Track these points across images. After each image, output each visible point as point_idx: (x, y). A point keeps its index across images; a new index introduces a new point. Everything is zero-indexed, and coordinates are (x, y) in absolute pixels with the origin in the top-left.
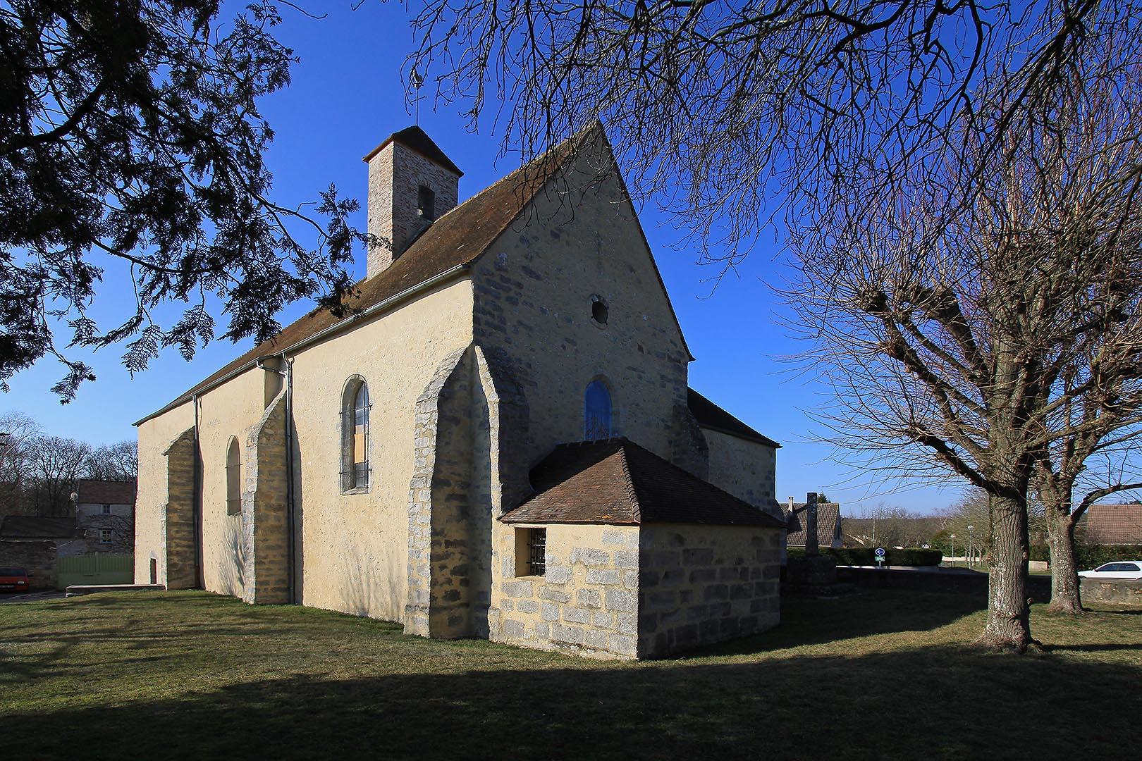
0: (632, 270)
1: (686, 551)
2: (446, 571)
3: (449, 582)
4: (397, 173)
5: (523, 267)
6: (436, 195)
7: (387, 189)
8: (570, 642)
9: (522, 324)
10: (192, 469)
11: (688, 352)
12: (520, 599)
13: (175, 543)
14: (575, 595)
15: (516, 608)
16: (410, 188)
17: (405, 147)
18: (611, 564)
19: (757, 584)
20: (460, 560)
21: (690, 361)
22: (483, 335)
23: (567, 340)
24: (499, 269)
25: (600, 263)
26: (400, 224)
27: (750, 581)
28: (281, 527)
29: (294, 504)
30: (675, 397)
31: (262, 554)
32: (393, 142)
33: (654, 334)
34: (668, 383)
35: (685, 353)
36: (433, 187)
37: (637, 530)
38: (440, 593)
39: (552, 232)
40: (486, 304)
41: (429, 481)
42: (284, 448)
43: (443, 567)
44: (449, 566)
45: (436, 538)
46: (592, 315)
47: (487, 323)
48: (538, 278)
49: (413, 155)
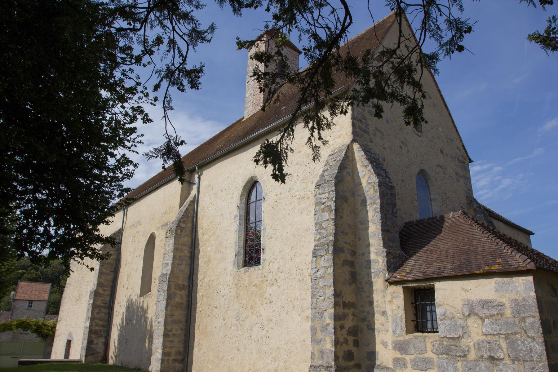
9: (377, 129)
10: (114, 262)
11: (468, 156)
12: (412, 357)
13: (95, 322)
14: (472, 348)
15: (409, 365)
18: (508, 313)
22: (358, 136)
28: (182, 303)
29: (193, 284)
31: (169, 328)
34: (460, 178)
35: (467, 157)
37: (530, 278)
38: (341, 354)
40: (358, 114)
41: (331, 248)
42: (190, 238)
43: (342, 327)
44: (345, 326)
47: (360, 128)
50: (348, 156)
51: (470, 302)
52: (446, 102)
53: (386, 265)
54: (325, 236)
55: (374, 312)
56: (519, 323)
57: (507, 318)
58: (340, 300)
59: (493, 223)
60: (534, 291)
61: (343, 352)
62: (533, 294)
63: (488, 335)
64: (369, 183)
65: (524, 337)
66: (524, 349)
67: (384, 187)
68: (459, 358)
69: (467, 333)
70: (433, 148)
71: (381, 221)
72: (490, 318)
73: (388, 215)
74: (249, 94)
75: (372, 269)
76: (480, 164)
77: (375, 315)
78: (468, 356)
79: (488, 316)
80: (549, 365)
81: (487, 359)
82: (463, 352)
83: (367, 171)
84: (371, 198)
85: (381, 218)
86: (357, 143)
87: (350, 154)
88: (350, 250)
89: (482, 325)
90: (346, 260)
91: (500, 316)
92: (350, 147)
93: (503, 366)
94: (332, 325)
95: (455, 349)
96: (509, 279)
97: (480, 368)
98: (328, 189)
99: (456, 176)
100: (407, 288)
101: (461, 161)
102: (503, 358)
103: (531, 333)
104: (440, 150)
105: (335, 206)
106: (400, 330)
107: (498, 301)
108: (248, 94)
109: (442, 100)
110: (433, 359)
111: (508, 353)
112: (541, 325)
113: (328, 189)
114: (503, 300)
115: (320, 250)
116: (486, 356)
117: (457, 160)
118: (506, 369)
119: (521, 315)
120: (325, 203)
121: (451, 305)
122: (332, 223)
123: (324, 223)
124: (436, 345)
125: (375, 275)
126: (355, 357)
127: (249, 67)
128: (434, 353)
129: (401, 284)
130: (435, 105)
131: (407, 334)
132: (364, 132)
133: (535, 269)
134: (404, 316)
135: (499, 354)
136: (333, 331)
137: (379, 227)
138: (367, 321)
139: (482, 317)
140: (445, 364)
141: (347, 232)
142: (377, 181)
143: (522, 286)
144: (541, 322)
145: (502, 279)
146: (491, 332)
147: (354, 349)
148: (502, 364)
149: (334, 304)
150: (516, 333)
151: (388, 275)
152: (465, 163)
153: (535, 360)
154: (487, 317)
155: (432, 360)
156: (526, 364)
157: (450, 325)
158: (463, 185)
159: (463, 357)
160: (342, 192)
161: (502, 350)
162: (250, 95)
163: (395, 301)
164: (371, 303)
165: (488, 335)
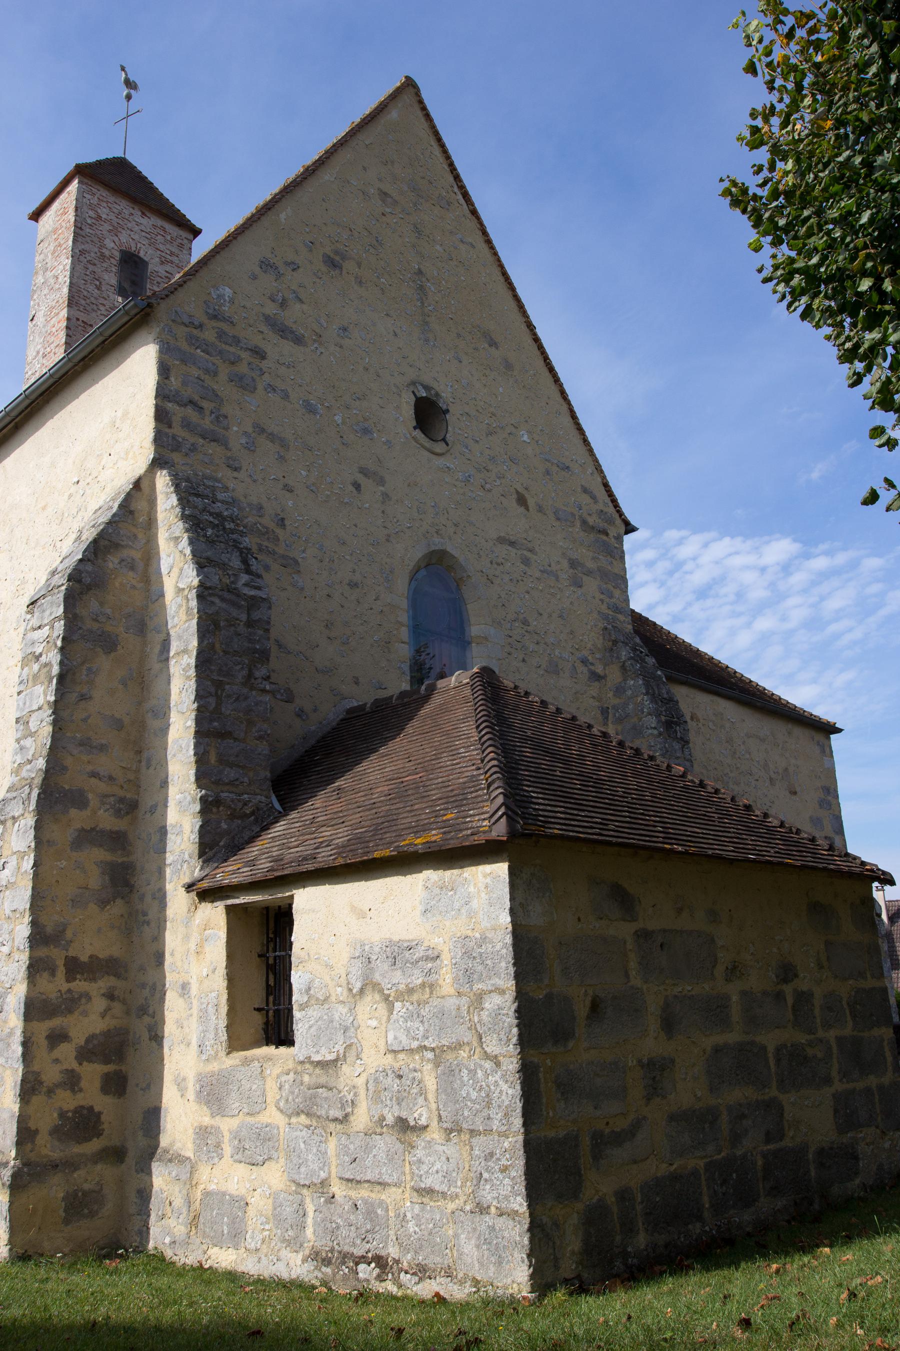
0: (493, 344)
1: (643, 935)
2: (67, 1052)
3: (72, 1081)
4: (81, 228)
5: (267, 319)
6: (150, 267)
7: (63, 257)
8: (358, 1252)
9: (263, 431)
11: (620, 513)
14: (362, 1092)
15: (228, 1150)
16: (103, 255)
17: (99, 188)
18: (446, 980)
19: (839, 1039)
20: (103, 1015)
21: (627, 532)
22: (177, 447)
23: (364, 471)
24: (215, 317)
25: (427, 323)
26: (83, 316)
27: (821, 1034)
30: (604, 608)
32: (76, 181)
33: (548, 472)
34: (585, 578)
35: (617, 516)
36: (146, 253)
37: (501, 869)
38: (45, 1121)
39: (325, 255)
40: (184, 383)
43: (57, 1038)
44: (72, 1033)
45: (43, 952)
46: (414, 423)
47: (187, 424)
48: (298, 340)
49: (112, 199)
50: (132, 512)
51: (367, 948)
52: (550, 357)
53: (197, 840)
54: (30, 758)
55: (165, 985)
56: (468, 1012)
57: (443, 997)
58: (58, 956)
59: (677, 702)
60: (507, 911)
61: (55, 1115)
62: (506, 919)
63: (398, 1052)
64: (180, 590)
65: (476, 1057)
66: (474, 1095)
67: (223, 599)
68: (332, 1126)
69: (354, 1047)
70: (490, 491)
71: (196, 705)
72: (406, 998)
73: (227, 687)
74: (34, 354)
75: (168, 855)
76: (826, 553)
77: (168, 994)
78: (352, 1118)
79: (402, 993)
80: (527, 1144)
81: (393, 1127)
82: (343, 1107)
83: (178, 554)
84: (180, 637)
85: (197, 695)
86: (165, 472)
87: (140, 505)
88: (112, 799)
89: (389, 1020)
90: (93, 829)
91: (427, 989)
92: (144, 485)
93: (425, 1148)
94: (18, 1037)
95: (326, 1099)
96: (456, 872)
97: (375, 1156)
98: (51, 614)
99: (572, 570)
100: (244, 907)
101: (593, 528)
102: (425, 1124)
103: (493, 1046)
104: (515, 496)
105: (61, 663)
106: (213, 1042)
107: (426, 944)
108: (31, 353)
109: (539, 353)
110: (278, 1128)
111: (438, 1109)
112: (517, 1018)
113: (51, 614)
114: (437, 941)
115: (12, 802)
116: (390, 1119)
117: (578, 524)
118: (432, 1159)
119: (475, 987)
120: (41, 655)
121: (326, 959)
122: (46, 715)
123: (35, 716)
124: (287, 1086)
125: (173, 873)
126: (105, 1126)
127: (36, 273)
128: (281, 1111)
129: (222, 899)
130: (509, 366)
131: (228, 1053)
132: (204, 439)
133: (505, 838)
134: (224, 997)
135: (418, 1112)
136: (19, 1050)
137: (191, 723)
138: (148, 1015)
139: (389, 996)
140: (302, 1146)
141: (103, 742)
142: (196, 582)
143: (483, 895)
144: (519, 1007)
145: (440, 872)
146: (406, 1042)
147: (102, 1103)
148: (423, 1144)
149: (30, 967)
150: (459, 1045)
151: (200, 870)
152: (607, 534)
153: (495, 1128)
154: (400, 996)
155: (275, 1131)
156: (474, 1141)
157: (320, 1023)
158: (594, 597)
159: (341, 1122)
160: (96, 620)
161: (426, 1099)
162: (36, 357)
163: (208, 948)
164: (160, 958)
165: (398, 1052)
